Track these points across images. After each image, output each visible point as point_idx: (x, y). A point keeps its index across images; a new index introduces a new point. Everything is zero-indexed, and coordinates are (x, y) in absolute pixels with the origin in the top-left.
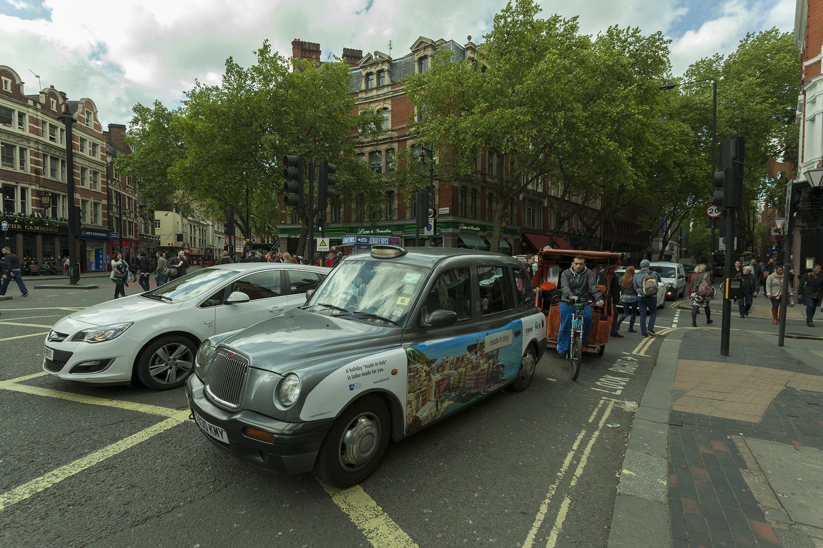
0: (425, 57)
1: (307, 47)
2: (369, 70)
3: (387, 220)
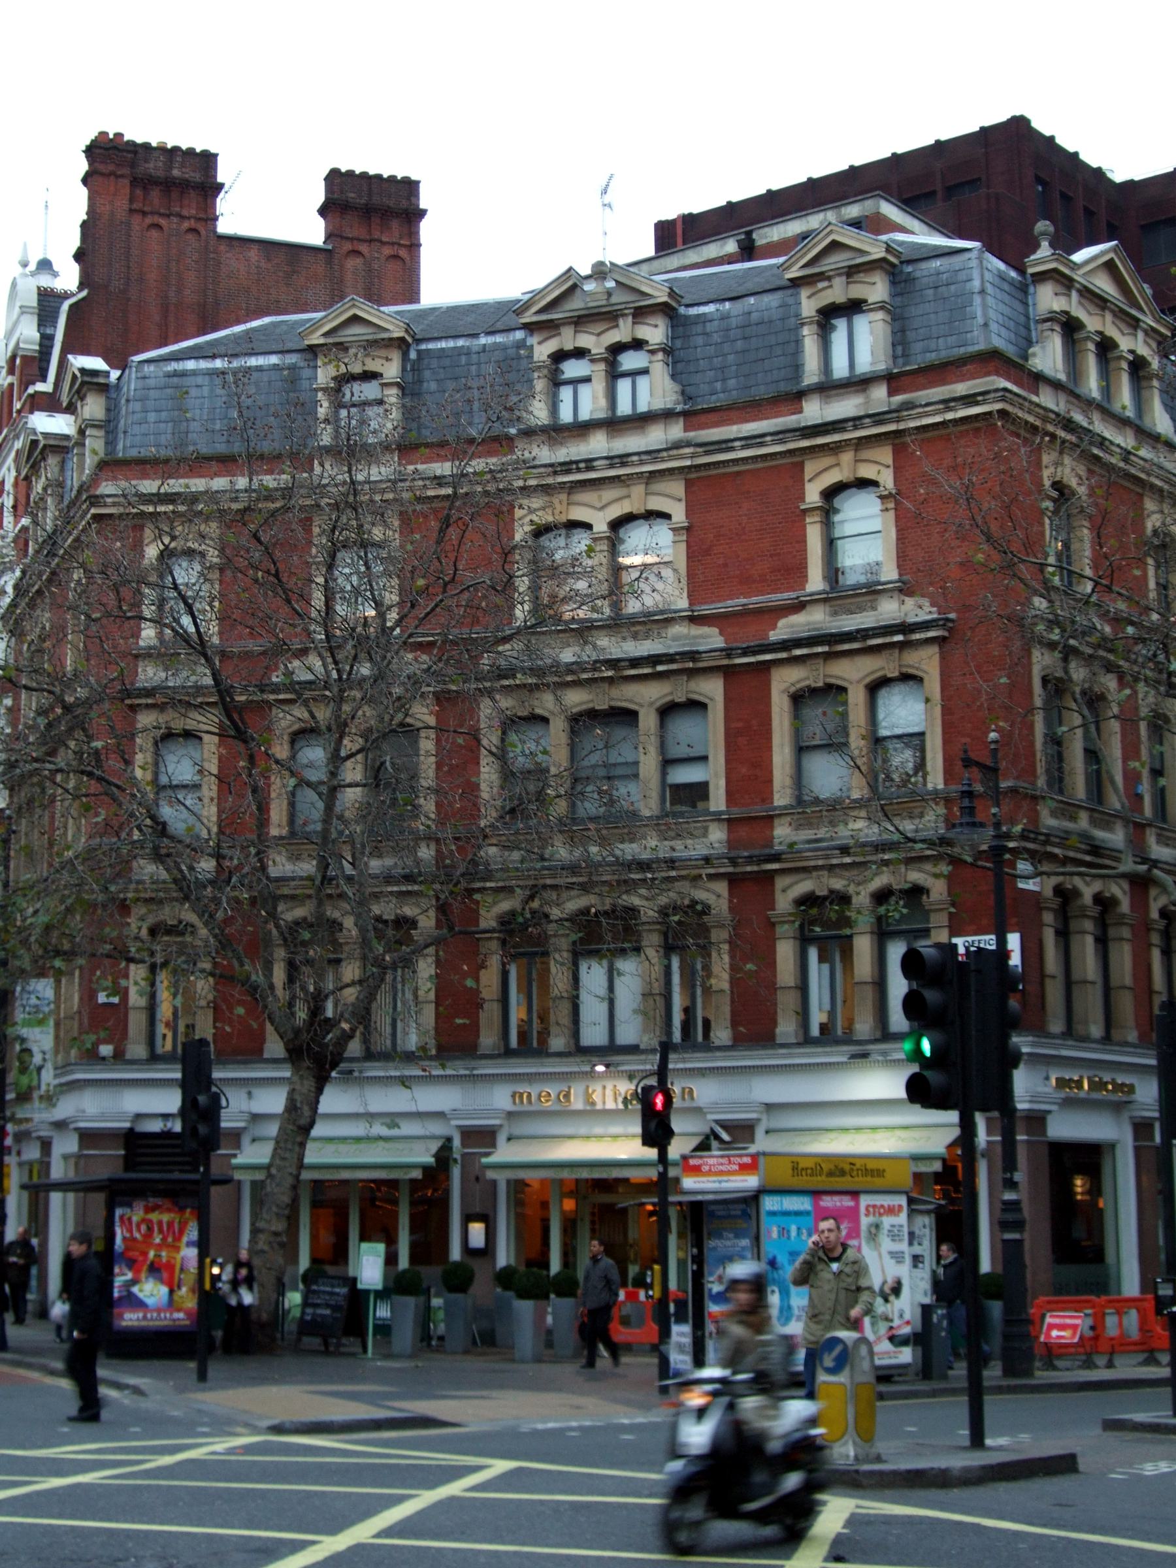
0: (854, 307)
1: (154, 167)
2: (568, 339)
3: (508, 1053)
